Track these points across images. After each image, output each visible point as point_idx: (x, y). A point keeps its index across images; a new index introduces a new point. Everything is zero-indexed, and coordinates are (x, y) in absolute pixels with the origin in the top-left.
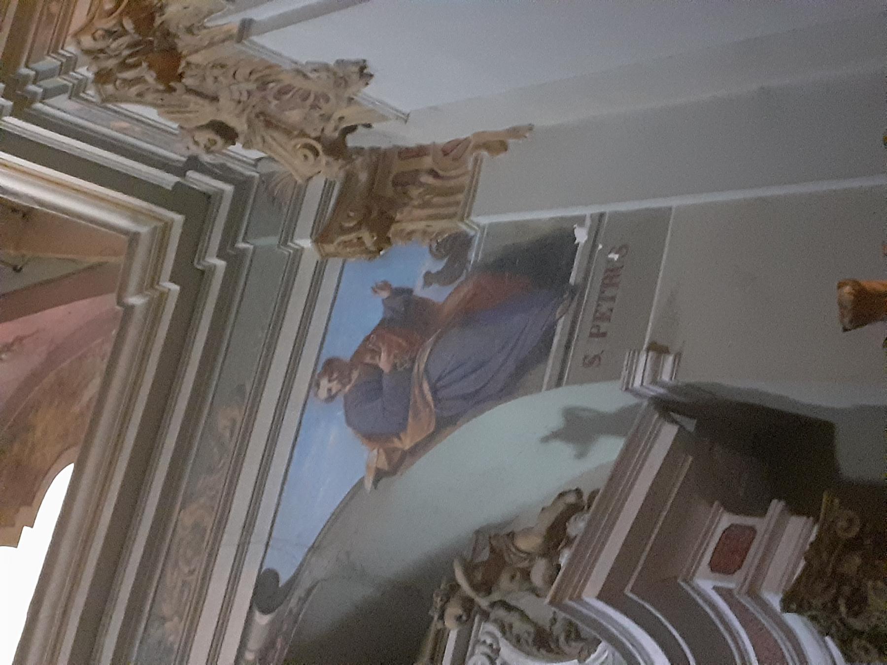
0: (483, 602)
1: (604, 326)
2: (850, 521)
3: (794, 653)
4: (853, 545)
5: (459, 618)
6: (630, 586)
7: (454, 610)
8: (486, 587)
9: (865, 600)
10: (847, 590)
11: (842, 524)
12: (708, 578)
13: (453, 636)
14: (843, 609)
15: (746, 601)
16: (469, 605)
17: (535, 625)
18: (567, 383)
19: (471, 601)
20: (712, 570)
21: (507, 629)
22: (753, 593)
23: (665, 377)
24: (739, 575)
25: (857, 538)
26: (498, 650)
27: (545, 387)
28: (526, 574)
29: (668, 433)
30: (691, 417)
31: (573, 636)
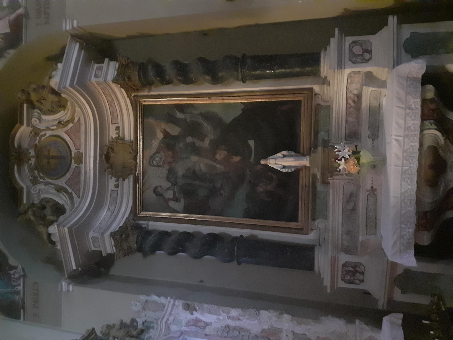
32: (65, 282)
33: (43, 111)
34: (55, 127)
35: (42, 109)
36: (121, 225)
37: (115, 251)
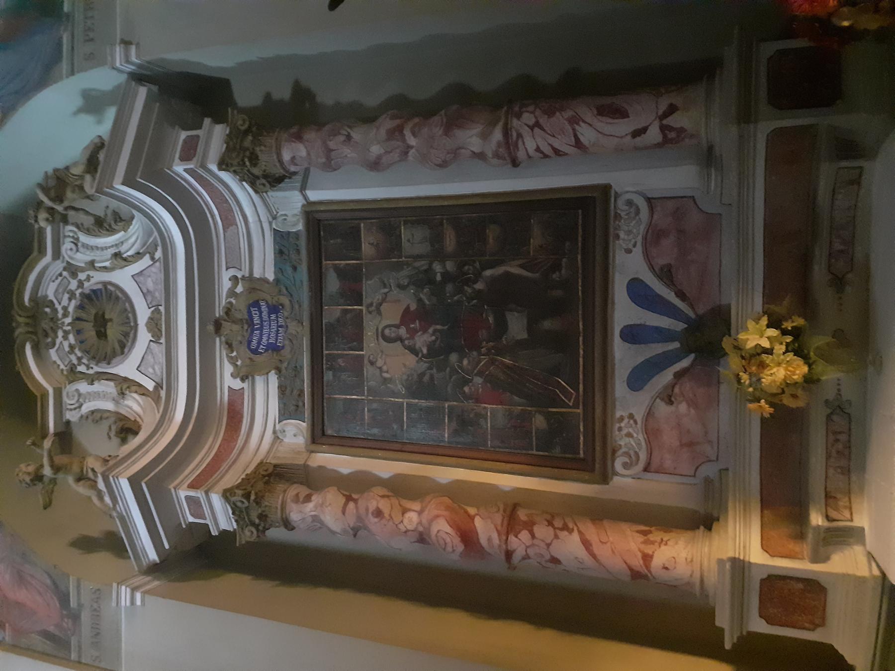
0: (59, 208)
1: (91, 35)
2: (244, 121)
3: (230, 195)
4: (246, 132)
5: (47, 220)
6: (139, 174)
7: (43, 215)
8: (59, 199)
9: (257, 157)
10: (248, 153)
11: (240, 122)
12: (180, 165)
13: (49, 230)
14: (248, 163)
15: (200, 171)
16: (51, 210)
17: (94, 215)
18: (78, 72)
19: (53, 209)
20: (181, 161)
21: (80, 226)
22: (203, 166)
23: (134, 59)
24: (195, 159)
25: (249, 127)
26: (78, 239)
27: (64, 76)
28: (81, 188)
29: (143, 92)
30: (155, 84)
31: (118, 220)
32: (134, 590)
33: (84, 228)
34: (107, 264)
35: (82, 224)
36: (249, 471)
37: (235, 527)
